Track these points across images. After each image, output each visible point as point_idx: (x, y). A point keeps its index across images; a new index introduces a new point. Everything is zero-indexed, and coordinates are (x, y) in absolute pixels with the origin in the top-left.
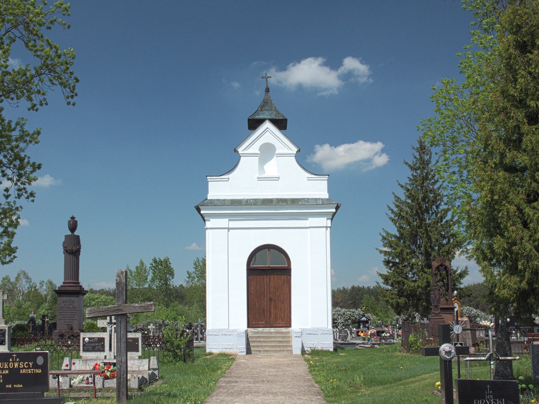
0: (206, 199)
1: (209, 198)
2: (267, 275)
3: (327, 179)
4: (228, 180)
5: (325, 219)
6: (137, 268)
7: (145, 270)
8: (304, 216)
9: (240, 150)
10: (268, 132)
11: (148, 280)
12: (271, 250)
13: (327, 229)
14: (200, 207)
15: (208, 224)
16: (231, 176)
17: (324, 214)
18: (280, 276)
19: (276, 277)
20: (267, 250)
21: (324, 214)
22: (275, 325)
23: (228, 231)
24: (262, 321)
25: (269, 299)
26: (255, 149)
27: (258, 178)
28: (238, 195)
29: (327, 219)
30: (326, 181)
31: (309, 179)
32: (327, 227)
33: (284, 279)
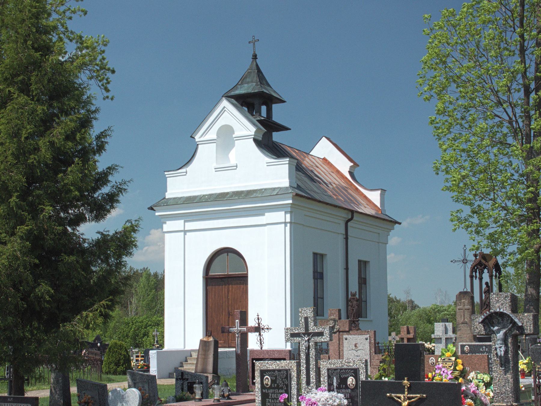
0: (165, 198)
1: (167, 197)
4: (235, 168)
8: (260, 212)
10: (226, 112)
12: (229, 254)
13: (286, 226)
14: (154, 208)
15: (166, 228)
16: (190, 168)
17: (285, 206)
18: (239, 286)
20: (226, 254)
21: (285, 206)
25: (227, 313)
26: (212, 135)
27: (215, 169)
28: (195, 191)
29: (286, 213)
30: (287, 165)
31: (269, 165)
32: (285, 223)
33: (243, 289)
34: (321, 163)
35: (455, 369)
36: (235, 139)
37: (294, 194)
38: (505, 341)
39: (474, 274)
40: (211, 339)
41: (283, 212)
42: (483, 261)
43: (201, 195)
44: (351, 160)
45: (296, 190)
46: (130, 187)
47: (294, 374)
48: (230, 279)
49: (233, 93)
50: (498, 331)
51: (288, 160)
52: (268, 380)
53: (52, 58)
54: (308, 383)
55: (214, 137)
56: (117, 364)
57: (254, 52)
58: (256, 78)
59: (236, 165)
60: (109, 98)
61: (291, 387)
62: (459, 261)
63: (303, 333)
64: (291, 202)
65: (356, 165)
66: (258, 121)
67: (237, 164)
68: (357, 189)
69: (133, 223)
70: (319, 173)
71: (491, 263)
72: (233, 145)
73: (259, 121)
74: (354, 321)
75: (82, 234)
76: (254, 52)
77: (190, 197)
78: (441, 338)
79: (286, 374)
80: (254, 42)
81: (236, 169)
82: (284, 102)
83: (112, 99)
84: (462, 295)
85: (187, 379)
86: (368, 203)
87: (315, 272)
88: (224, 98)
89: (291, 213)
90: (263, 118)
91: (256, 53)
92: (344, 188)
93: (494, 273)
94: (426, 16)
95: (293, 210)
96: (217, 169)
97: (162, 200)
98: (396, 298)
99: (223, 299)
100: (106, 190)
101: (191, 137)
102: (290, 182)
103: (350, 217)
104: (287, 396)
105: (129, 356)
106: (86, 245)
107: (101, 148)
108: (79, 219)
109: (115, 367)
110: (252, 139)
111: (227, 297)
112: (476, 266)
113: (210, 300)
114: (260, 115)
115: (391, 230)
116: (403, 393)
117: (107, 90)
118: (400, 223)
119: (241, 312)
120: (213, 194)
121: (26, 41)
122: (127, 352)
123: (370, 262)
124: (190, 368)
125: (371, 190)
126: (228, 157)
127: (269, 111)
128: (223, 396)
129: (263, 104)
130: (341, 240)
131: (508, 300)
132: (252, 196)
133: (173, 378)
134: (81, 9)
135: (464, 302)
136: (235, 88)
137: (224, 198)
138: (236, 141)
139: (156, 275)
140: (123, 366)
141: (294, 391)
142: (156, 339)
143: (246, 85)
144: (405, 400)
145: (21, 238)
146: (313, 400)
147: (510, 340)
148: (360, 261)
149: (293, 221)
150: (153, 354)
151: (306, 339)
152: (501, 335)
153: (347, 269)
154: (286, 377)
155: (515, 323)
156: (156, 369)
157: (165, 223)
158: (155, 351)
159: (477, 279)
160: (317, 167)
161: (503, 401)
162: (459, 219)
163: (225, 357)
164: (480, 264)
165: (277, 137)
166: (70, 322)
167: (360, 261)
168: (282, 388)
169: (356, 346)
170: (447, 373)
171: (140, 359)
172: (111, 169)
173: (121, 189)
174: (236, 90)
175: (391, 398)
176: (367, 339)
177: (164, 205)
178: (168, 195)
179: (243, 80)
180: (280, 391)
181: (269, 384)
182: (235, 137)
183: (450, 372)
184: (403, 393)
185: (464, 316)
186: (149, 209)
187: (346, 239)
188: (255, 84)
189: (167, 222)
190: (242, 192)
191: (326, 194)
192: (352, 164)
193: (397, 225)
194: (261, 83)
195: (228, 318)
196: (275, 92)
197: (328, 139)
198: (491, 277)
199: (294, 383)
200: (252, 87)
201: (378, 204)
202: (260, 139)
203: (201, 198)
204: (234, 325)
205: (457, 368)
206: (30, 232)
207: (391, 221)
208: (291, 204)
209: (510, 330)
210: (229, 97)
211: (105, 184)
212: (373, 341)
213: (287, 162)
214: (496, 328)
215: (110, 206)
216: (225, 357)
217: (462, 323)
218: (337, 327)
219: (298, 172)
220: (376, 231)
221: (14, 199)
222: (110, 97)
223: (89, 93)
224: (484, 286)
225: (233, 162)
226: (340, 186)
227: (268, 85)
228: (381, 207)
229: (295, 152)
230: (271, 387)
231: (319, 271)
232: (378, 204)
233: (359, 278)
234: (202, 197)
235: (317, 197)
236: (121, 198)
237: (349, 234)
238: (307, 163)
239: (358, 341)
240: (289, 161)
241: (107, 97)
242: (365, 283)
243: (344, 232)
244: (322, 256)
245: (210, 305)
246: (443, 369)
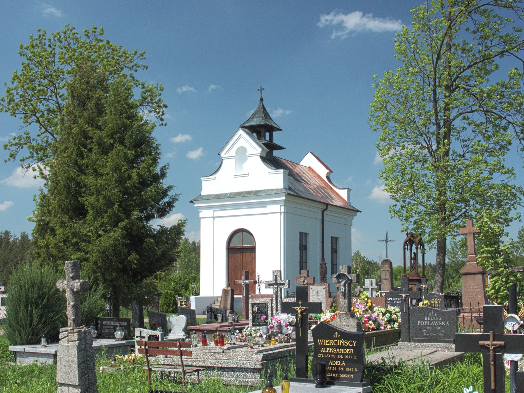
0: (201, 195)
1: (202, 195)
2: (241, 253)
5: (279, 205)
12: (244, 233)
13: (281, 214)
14: (194, 202)
19: (247, 254)
23: (214, 219)
26: (233, 153)
29: (281, 206)
30: (282, 174)
31: (270, 173)
32: (281, 213)
34: (307, 171)
35: (366, 305)
37: (287, 193)
38: (344, 285)
39: (406, 247)
40: (229, 288)
42: (412, 239)
44: (327, 168)
45: (288, 191)
46: (180, 198)
47: (269, 305)
48: (244, 250)
49: (246, 125)
50: (342, 281)
52: (256, 309)
53: (137, 123)
54: (277, 310)
55: (234, 155)
56: (168, 306)
57: (261, 97)
58: (262, 115)
61: (268, 313)
62: (384, 241)
63: (275, 284)
65: (331, 171)
66: (263, 143)
68: (331, 188)
69: (183, 221)
70: (305, 178)
71: (417, 240)
72: (247, 159)
73: (264, 144)
74: (323, 278)
75: (152, 226)
76: (261, 97)
77: (218, 194)
78: (368, 288)
79: (265, 305)
80: (261, 90)
82: (281, 130)
83: (166, 125)
84: (385, 262)
85: (214, 312)
86: (339, 198)
87: (301, 245)
88: (240, 129)
89: (284, 205)
90: (266, 142)
91: (263, 97)
92: (322, 188)
93: (419, 247)
94: (374, 76)
95: (286, 203)
98: (373, 261)
100: (166, 200)
101: (219, 154)
102: (284, 186)
103: (325, 208)
104: (265, 317)
105: (176, 301)
106: (156, 233)
107: (163, 175)
108: (150, 217)
109: (167, 308)
112: (407, 241)
113: (230, 264)
114: (265, 139)
115: (354, 216)
116: (299, 307)
117: (162, 120)
118: (360, 212)
119: (246, 272)
120: (233, 193)
121: (121, 114)
122: (175, 298)
123: (340, 239)
124: (217, 306)
125: (341, 189)
127: (271, 136)
128: (234, 321)
129: (267, 131)
130: (319, 223)
131: (347, 268)
133: (205, 314)
134: (143, 65)
135: (386, 266)
136: (248, 121)
137: (240, 195)
139: (194, 243)
140: (172, 307)
141: (269, 315)
142: (194, 290)
143: (255, 119)
144: (299, 310)
145: (122, 229)
146: (279, 319)
147: (347, 285)
148: (332, 238)
150: (193, 298)
151: (276, 287)
152: (343, 283)
153: (323, 243)
154: (265, 307)
155: (348, 278)
158: (194, 297)
159: (409, 250)
160: (304, 173)
161: (344, 311)
162: (394, 210)
164: (410, 240)
165: (276, 153)
166: (149, 277)
167: (332, 238)
168: (263, 313)
169: (317, 293)
170: (362, 308)
171: (183, 303)
172: (170, 188)
173: (174, 200)
175: (294, 309)
176: (324, 289)
178: (203, 193)
179: (253, 116)
180: (262, 314)
181: (256, 310)
183: (363, 307)
184: (299, 307)
185: (386, 274)
186: (190, 202)
187: (323, 222)
188: (261, 118)
190: (252, 192)
191: (309, 192)
192: (328, 171)
193: (358, 213)
194: (265, 118)
196: (275, 123)
197: (312, 153)
198: (417, 249)
199: (269, 310)
200: (259, 121)
201: (345, 198)
202: (265, 156)
203: (225, 195)
204: (241, 279)
205: (368, 305)
206: (125, 226)
207: (354, 210)
209: (347, 281)
210: (243, 127)
211: (166, 197)
212: (328, 290)
214: (341, 280)
215: (169, 209)
217: (385, 279)
218: (306, 281)
219: (290, 177)
221: (116, 206)
222: (164, 124)
223: (157, 143)
224: (413, 255)
225: (245, 172)
226: (320, 187)
227: (271, 119)
229: (289, 163)
230: (257, 313)
231: (303, 244)
232: (345, 198)
233: (331, 249)
235: (301, 194)
236: (175, 204)
237: (325, 219)
238: (297, 170)
239: (319, 290)
241: (162, 124)
242: (336, 252)
243: (321, 218)
244: (306, 234)
246: (360, 305)
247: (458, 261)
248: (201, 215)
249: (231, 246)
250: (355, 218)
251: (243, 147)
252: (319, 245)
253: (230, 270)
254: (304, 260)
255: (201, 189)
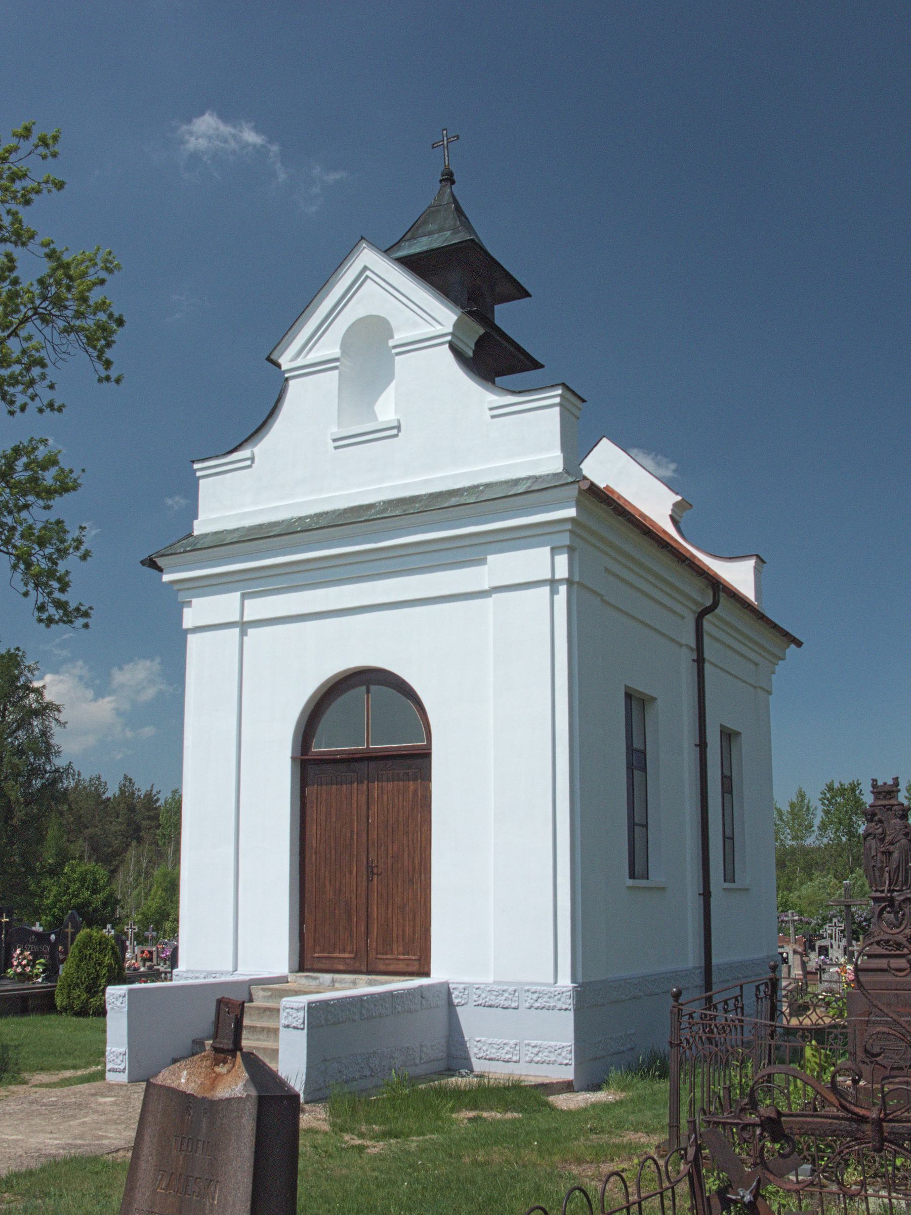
0: (190, 535)
1: (196, 533)
2: (360, 782)
3: (557, 400)
6: (792, 805)
7: (808, 809)
9: (286, 361)
10: (369, 281)
11: (815, 828)
12: (373, 688)
13: (554, 592)
14: (160, 562)
16: (262, 448)
18: (401, 783)
19: (389, 786)
20: (364, 688)
22: (382, 967)
24: (344, 951)
25: (364, 869)
27: (334, 440)
29: (554, 551)
30: (557, 410)
31: (497, 413)
32: (553, 583)
36: (394, 351)
41: (547, 549)
43: (292, 519)
51: (560, 392)
55: (336, 352)
59: (395, 424)
60: (112, 380)
64: (571, 512)
67: (399, 421)
81: (396, 436)
83: (118, 381)
96: (341, 442)
97: (184, 539)
99: (352, 823)
103: (709, 603)
109: (84, 996)
110: (447, 346)
111: (364, 819)
118: (799, 644)
123: (743, 737)
125: (730, 559)
126: (374, 412)
130: (686, 658)
132: (446, 505)
138: (397, 358)
149: (577, 579)
156: (124, 1049)
157: (189, 604)
163: (357, 1017)
174: (398, 250)
177: (185, 552)
178: (199, 528)
182: (395, 347)
186: (143, 563)
187: (700, 661)
189: (194, 601)
193: (793, 646)
195: (368, 880)
208: (572, 520)
213: (557, 400)
216: (357, 1017)
220: (752, 656)
222: (114, 377)
228: (756, 599)
234: (295, 522)
240: (561, 396)
241: (108, 378)
243: (693, 643)
245: (312, 841)
247: (784, 846)
248: (189, 619)
249: (318, 748)
250: (781, 666)
251: (379, 317)
252: (690, 755)
253: (311, 858)
254: (637, 819)
255: (193, 512)
